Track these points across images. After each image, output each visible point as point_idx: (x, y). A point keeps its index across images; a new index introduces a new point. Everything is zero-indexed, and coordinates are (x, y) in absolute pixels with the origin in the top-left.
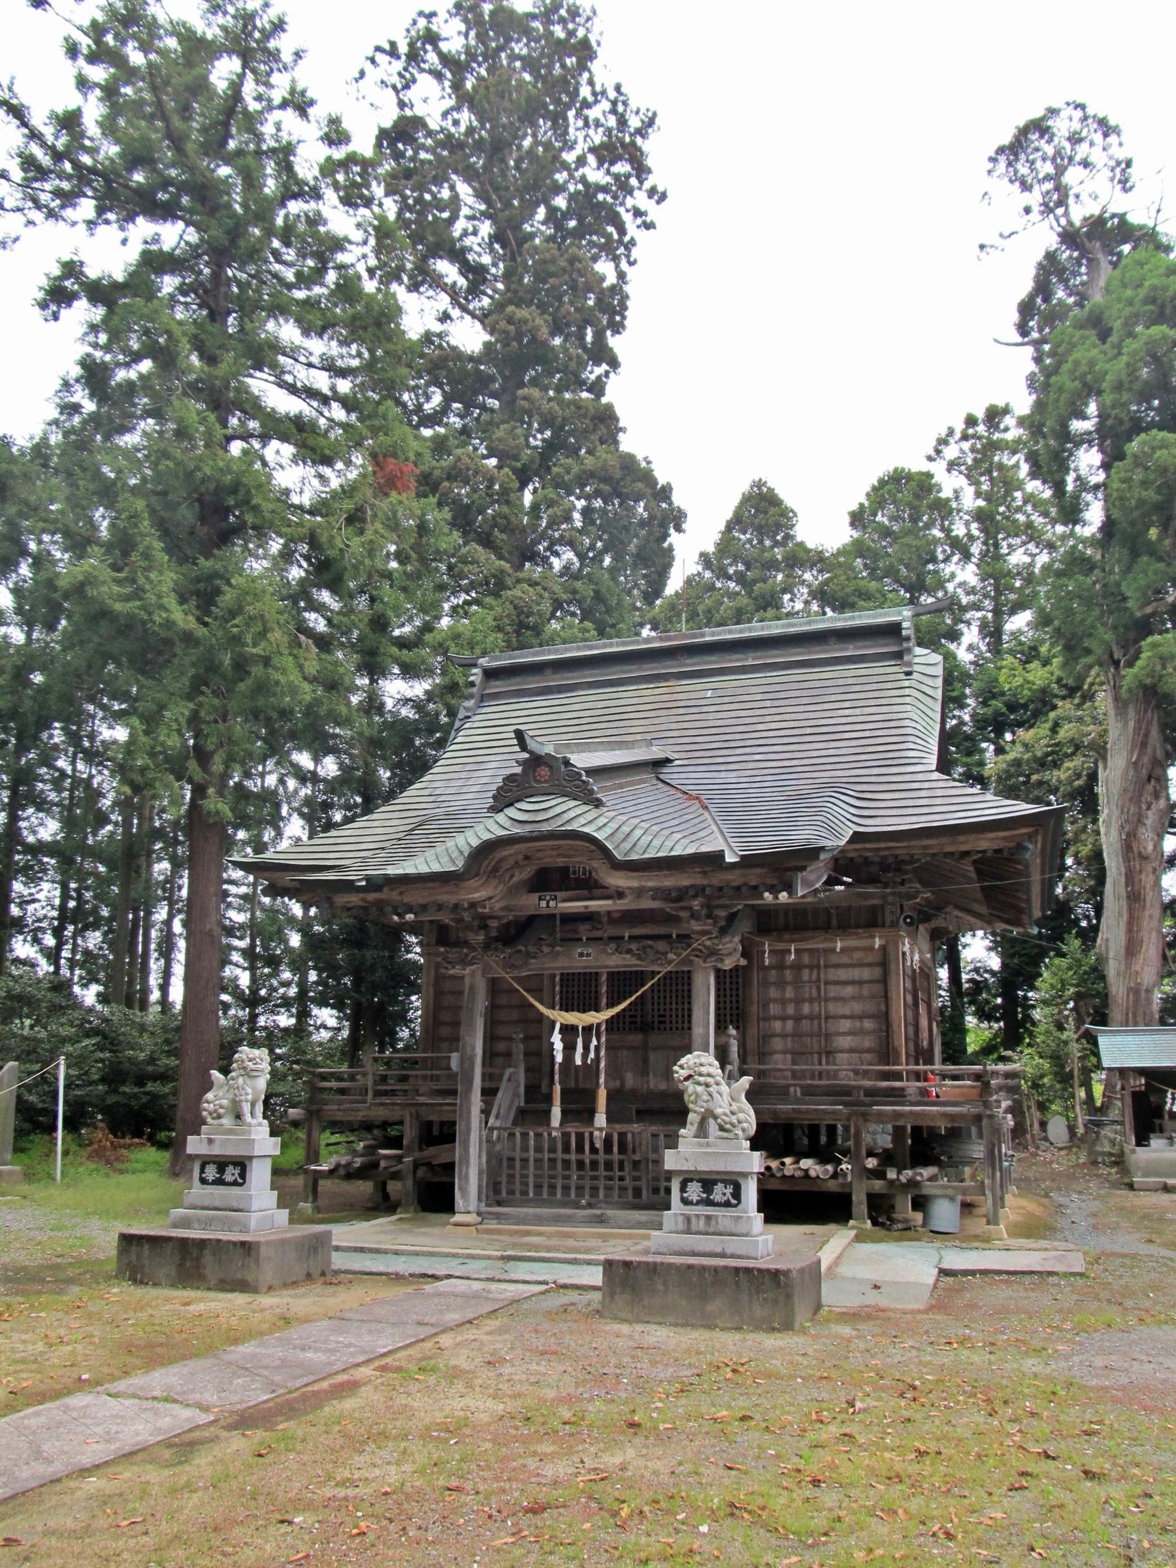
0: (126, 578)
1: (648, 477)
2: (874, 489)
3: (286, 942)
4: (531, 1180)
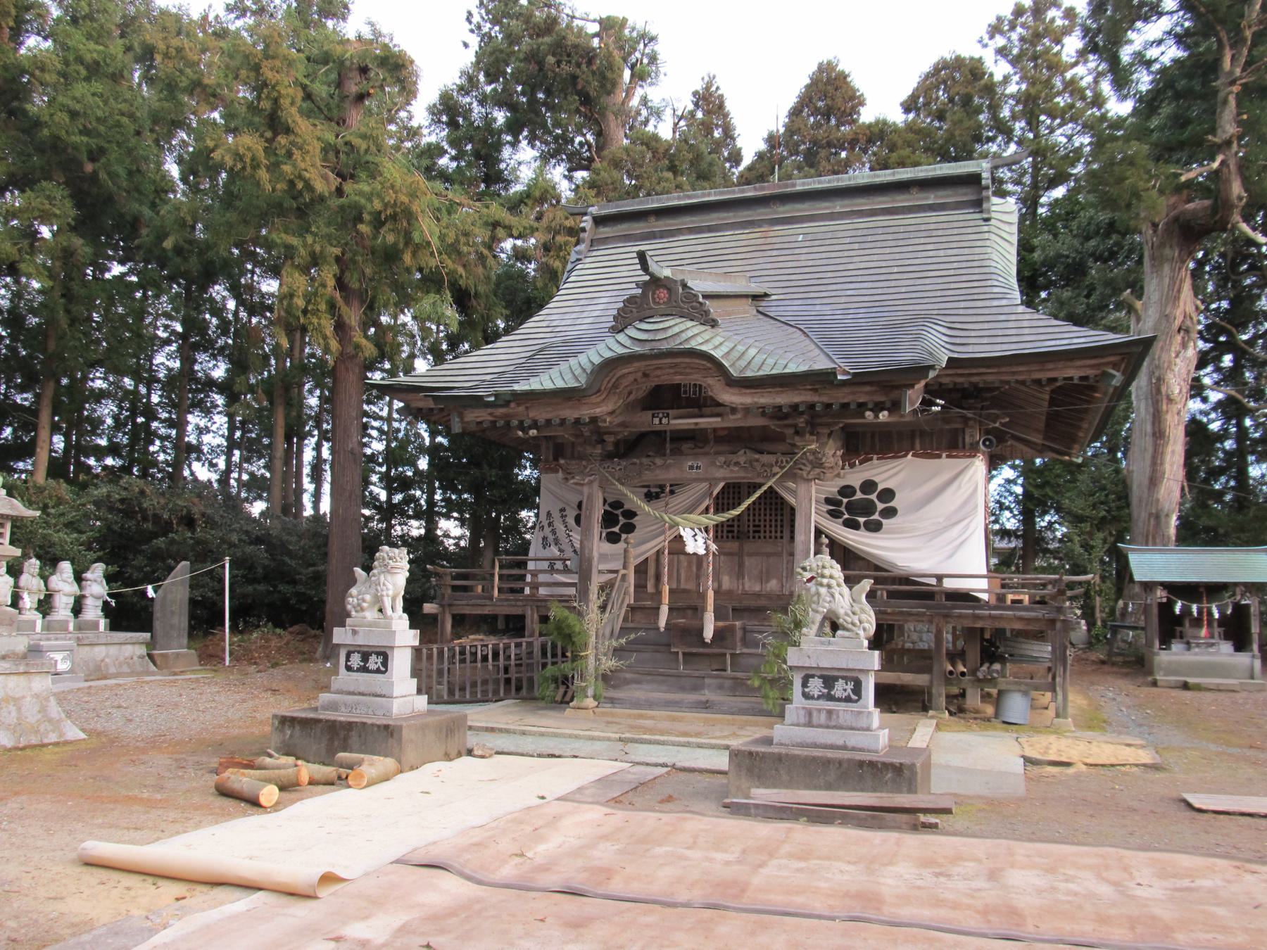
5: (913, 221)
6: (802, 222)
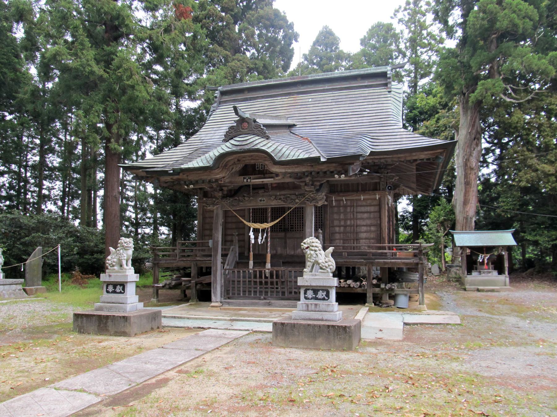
0: (74, 53)
1: (284, 19)
2: (370, 30)
3: (149, 202)
4: (241, 289)
5: (358, 93)
6: (311, 93)
